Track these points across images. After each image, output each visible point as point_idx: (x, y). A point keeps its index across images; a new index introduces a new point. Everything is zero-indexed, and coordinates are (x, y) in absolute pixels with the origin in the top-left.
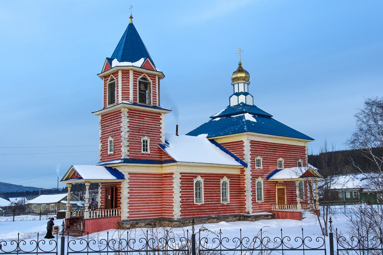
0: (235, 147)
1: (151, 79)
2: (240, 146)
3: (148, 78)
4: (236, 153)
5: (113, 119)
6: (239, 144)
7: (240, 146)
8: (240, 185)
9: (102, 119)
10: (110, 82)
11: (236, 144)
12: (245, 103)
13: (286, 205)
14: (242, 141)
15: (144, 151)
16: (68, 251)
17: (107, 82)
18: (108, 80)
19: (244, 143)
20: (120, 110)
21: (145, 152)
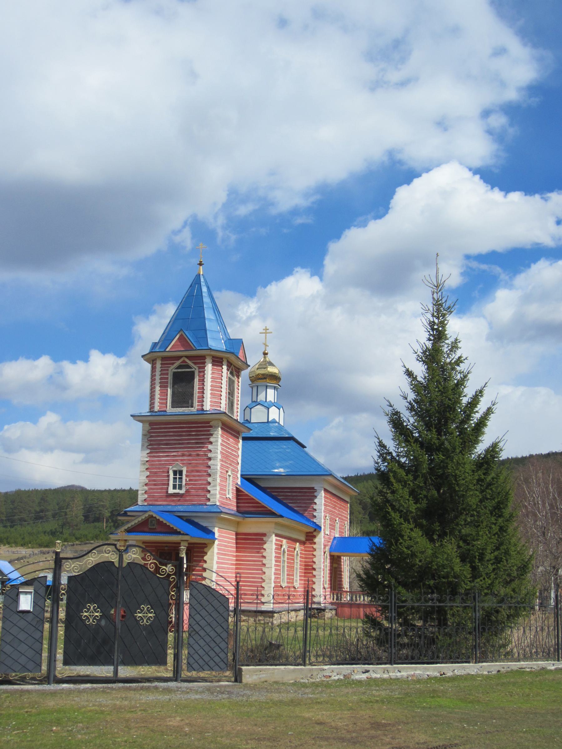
0: (296, 496)
1: (195, 363)
2: (308, 496)
3: (190, 363)
4: (298, 507)
5: (184, 434)
6: (306, 492)
7: (308, 496)
8: (237, 560)
9: (151, 430)
10: (177, 368)
11: (300, 492)
12: (283, 425)
13: (116, 672)
14: (313, 488)
15: (174, 487)
16: (208, 579)
17: (170, 367)
18: (173, 364)
19: (316, 492)
20: (208, 423)
21: (177, 491)
